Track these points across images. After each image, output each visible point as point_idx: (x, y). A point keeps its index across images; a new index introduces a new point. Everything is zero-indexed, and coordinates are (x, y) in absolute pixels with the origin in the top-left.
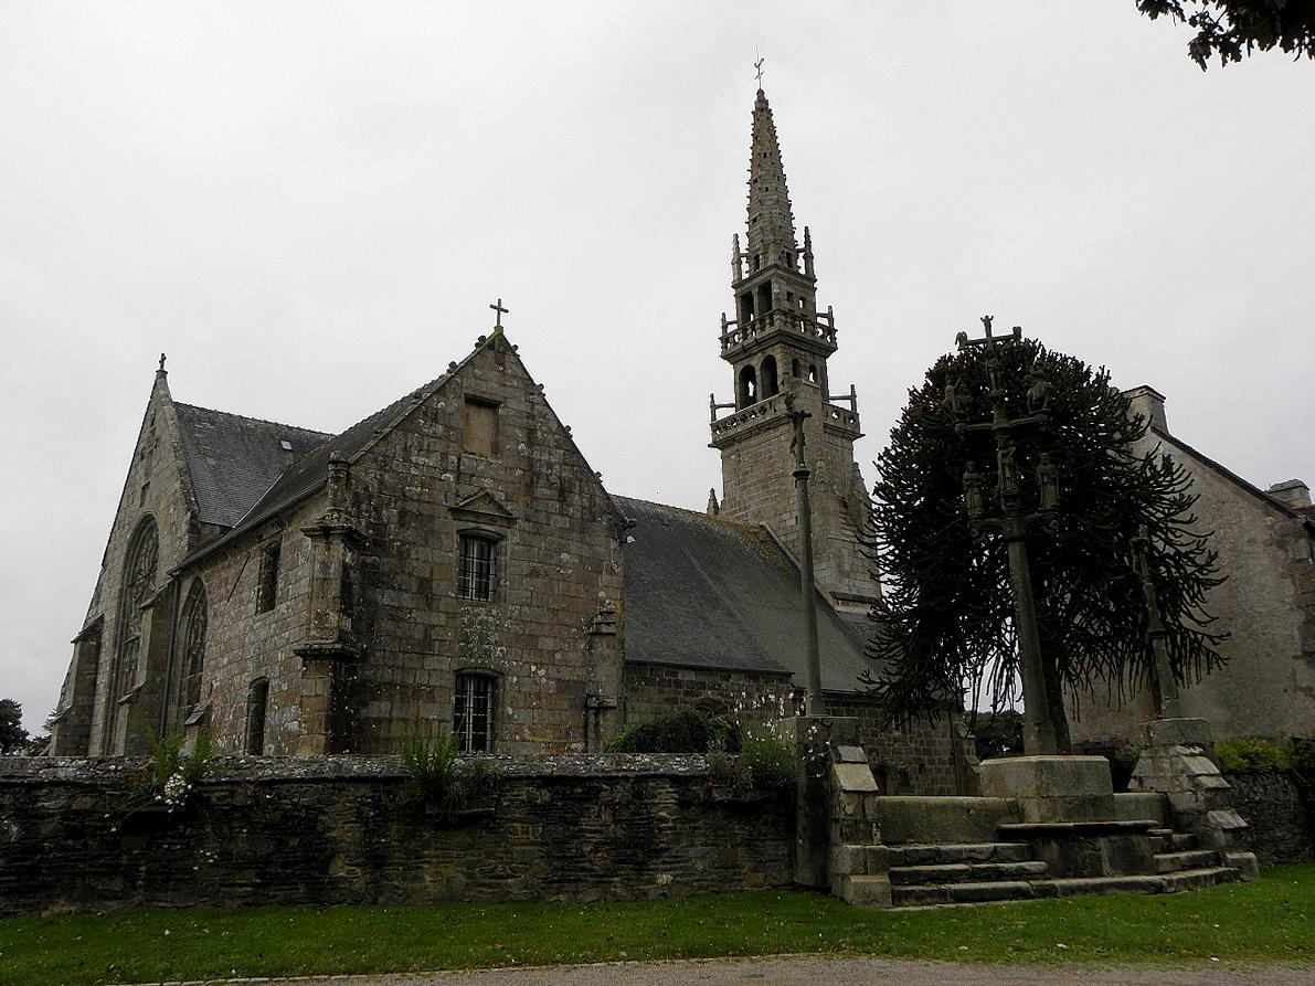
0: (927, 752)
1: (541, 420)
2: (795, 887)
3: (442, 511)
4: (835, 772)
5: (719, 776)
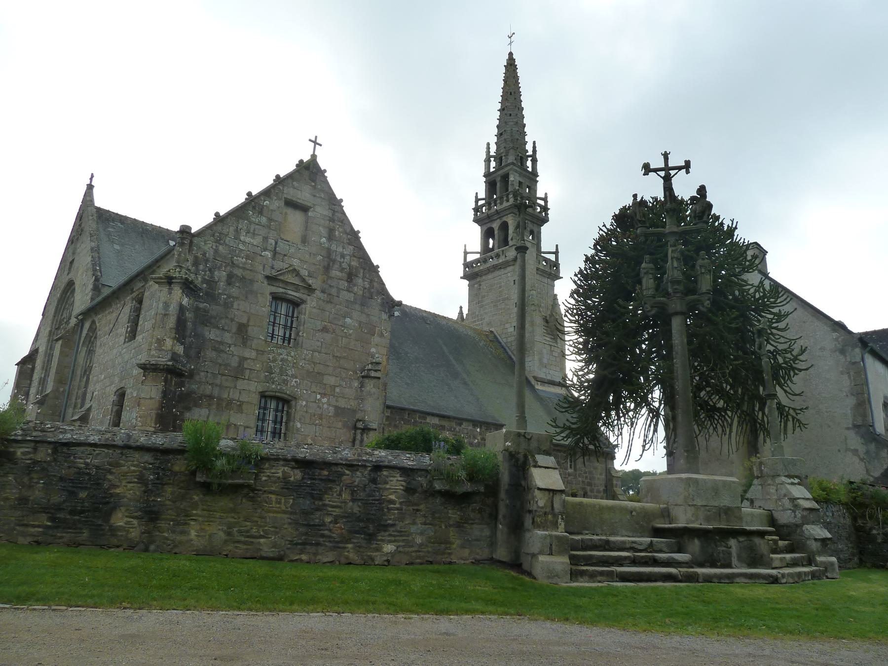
0: (590, 484)
2: (493, 561)
3: (260, 277)
4: (532, 475)
5: (436, 472)
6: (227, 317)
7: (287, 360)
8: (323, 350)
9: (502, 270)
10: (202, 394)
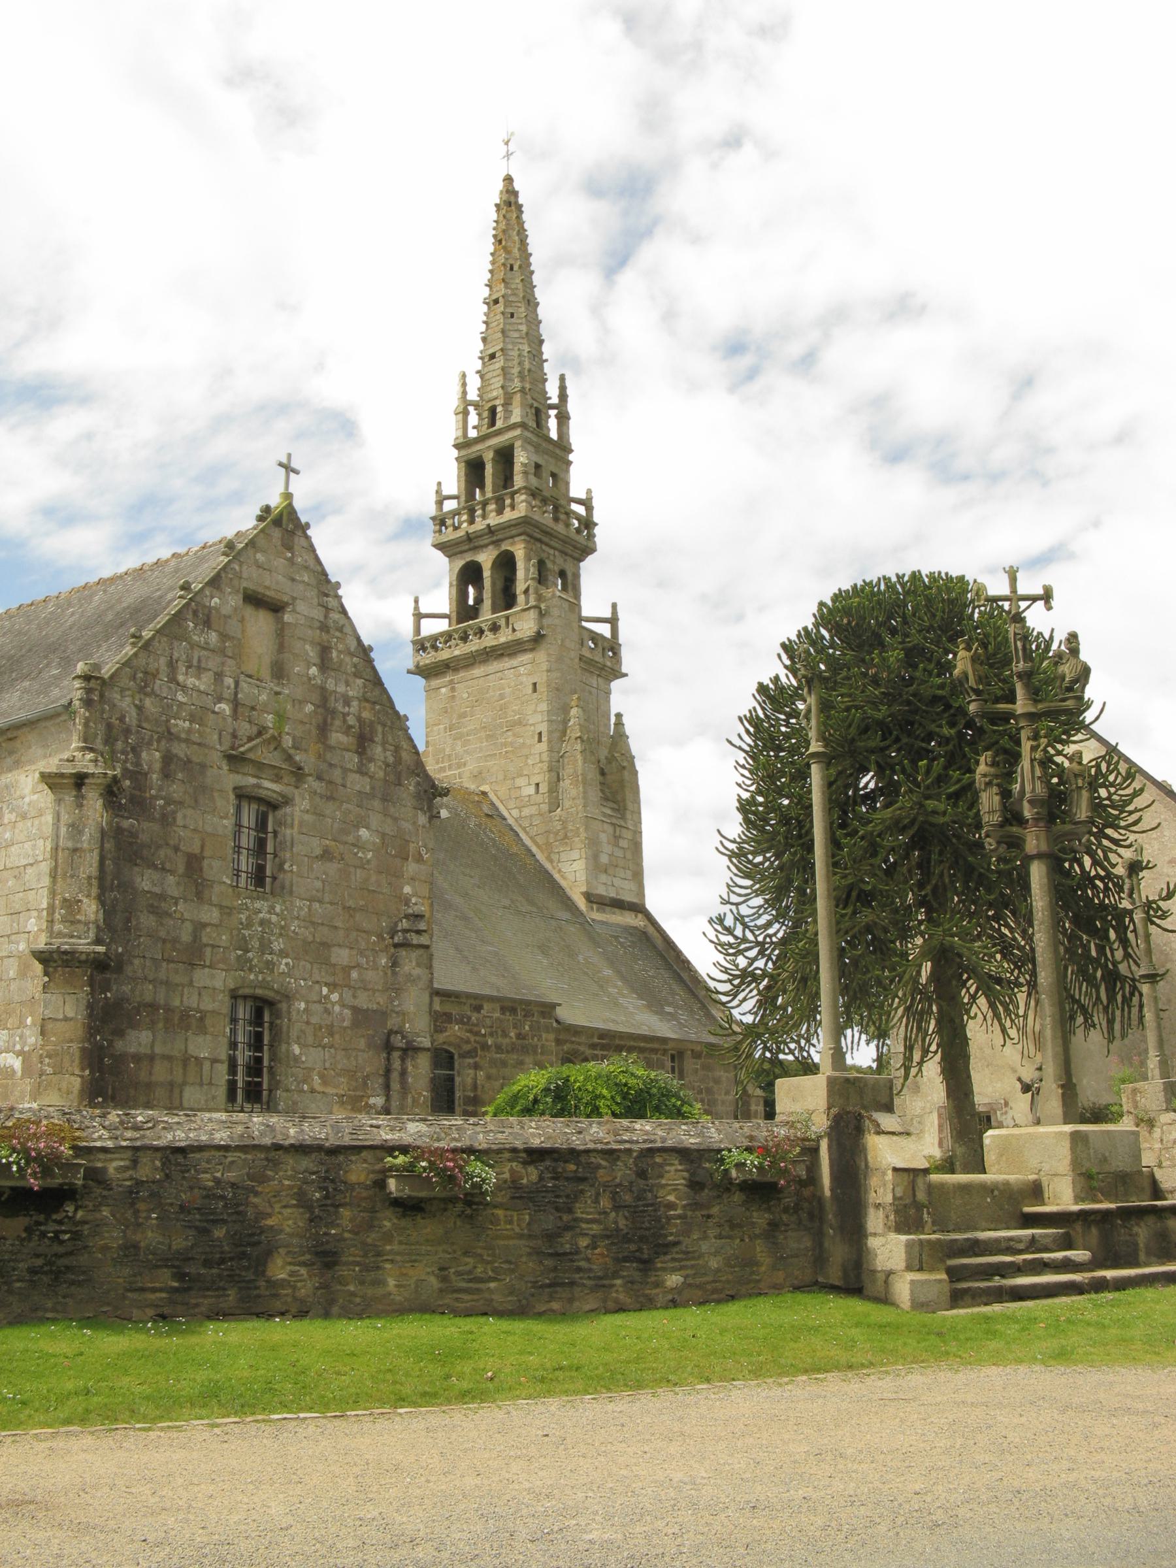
1: (338, 634)
3: (215, 757)
6: (167, 844)
7: (269, 921)
8: (327, 899)
9: (506, 659)
10: (139, 1003)
